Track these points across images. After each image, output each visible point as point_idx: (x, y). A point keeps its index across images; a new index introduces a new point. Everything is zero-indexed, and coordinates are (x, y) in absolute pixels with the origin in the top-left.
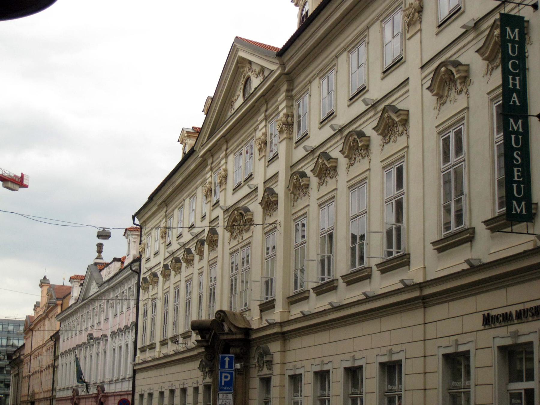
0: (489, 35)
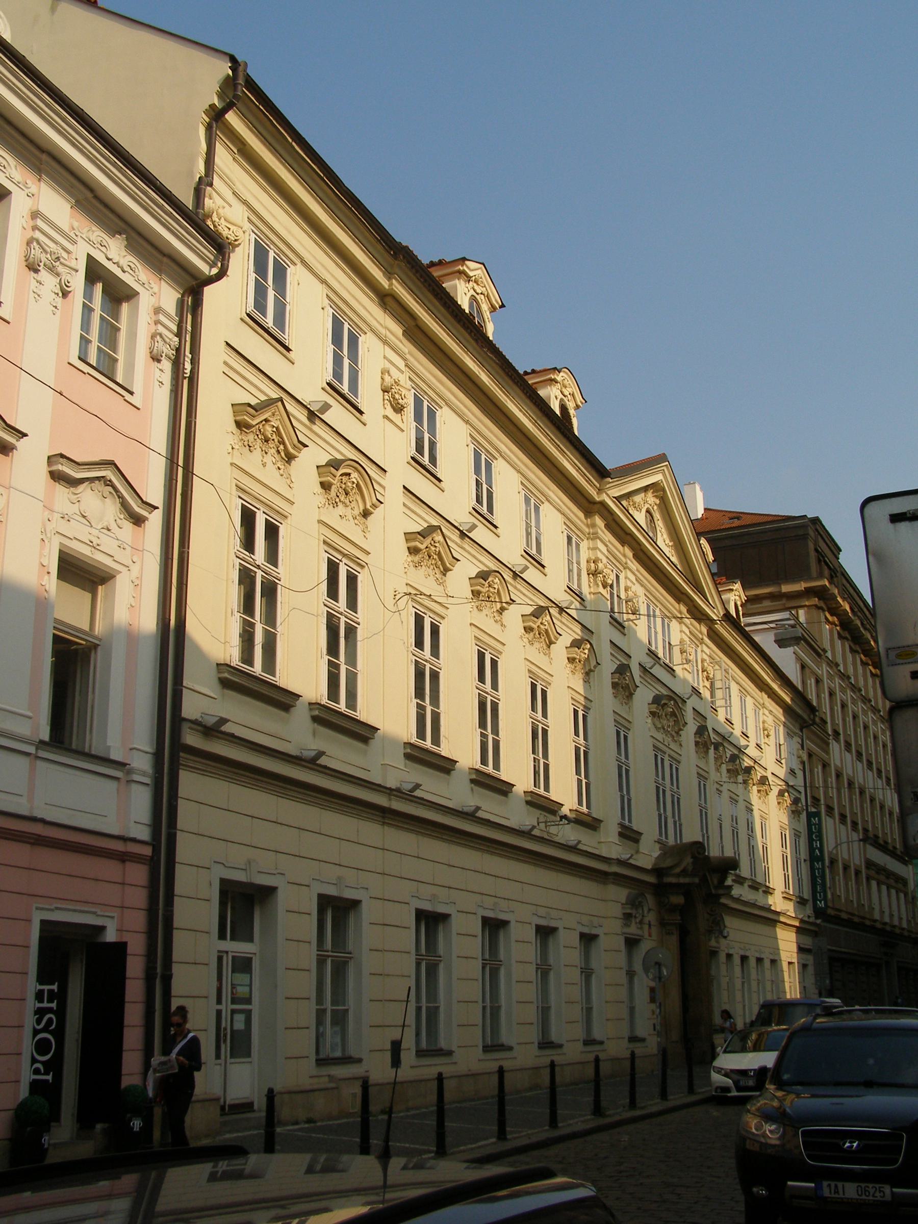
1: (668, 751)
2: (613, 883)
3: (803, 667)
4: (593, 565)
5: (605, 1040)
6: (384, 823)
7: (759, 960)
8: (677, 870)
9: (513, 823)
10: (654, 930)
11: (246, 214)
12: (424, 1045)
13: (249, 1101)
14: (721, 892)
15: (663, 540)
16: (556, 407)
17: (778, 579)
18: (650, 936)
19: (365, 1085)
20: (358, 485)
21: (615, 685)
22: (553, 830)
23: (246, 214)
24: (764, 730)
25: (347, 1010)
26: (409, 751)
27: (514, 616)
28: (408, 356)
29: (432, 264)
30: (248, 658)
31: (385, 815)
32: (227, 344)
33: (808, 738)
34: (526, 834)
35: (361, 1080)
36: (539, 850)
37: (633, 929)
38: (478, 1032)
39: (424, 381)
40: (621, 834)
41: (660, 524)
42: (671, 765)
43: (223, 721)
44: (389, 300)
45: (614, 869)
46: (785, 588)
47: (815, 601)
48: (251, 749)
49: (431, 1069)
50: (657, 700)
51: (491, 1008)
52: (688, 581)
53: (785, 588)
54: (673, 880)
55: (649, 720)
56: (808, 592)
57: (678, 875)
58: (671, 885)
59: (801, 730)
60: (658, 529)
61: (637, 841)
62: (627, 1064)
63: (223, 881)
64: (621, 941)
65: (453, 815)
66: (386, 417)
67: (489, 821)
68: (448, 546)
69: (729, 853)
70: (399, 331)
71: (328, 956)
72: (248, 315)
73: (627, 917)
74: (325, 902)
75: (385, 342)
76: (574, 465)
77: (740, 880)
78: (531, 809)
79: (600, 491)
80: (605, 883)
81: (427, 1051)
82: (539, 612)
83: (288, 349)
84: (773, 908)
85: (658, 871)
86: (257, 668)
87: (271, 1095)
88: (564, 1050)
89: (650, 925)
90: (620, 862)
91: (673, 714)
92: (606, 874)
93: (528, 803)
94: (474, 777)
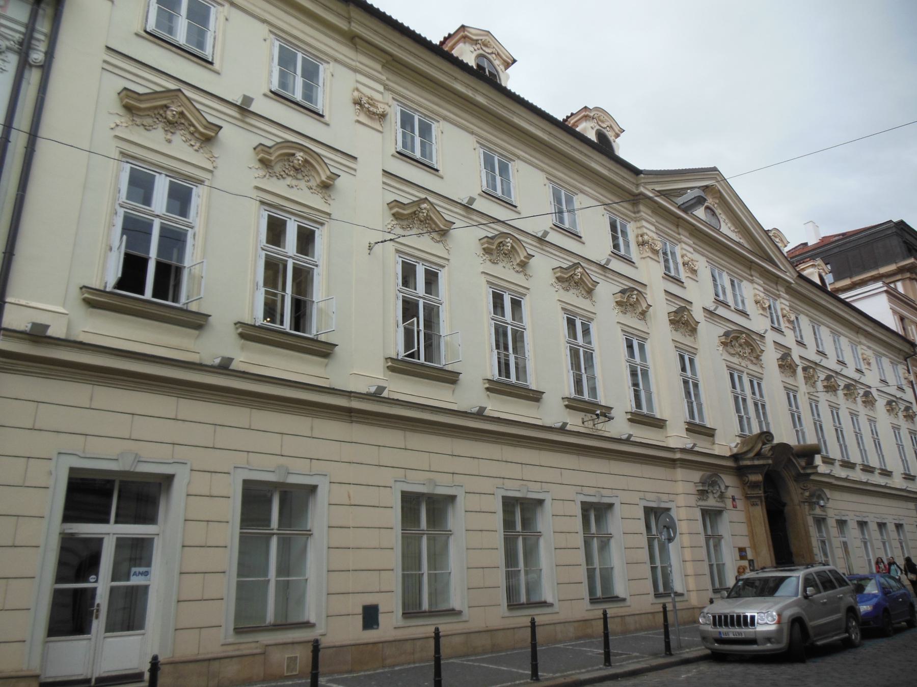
0: (414, 202)
1: (746, 371)
2: (681, 467)
3: (902, 319)
4: (640, 238)
5: (685, 593)
6: (352, 422)
7: (842, 523)
8: (751, 455)
9: (548, 422)
10: (740, 504)
11: (391, 96)
12: (717, 586)
13: (137, 671)
14: (809, 471)
15: (727, 229)
16: (592, 136)
17: (876, 266)
18: (735, 507)
19: (316, 647)
20: (306, 161)
21: (780, 366)
22: (599, 426)
23: (391, 96)
24: (864, 359)
25: (269, 581)
26: (390, 364)
27: (840, 393)
28: (387, 82)
29: (442, 43)
30: (638, 404)
31: (349, 415)
32: (108, 48)
33: (913, 365)
34: (562, 429)
35: (310, 644)
36: (381, 411)
37: (712, 502)
38: (708, 579)
39: (412, 101)
40: (687, 430)
41: (722, 217)
42: (751, 382)
43: (630, 436)
44: (357, 40)
45: (678, 456)
46: (883, 270)
47: (908, 275)
48: (18, 338)
49: (423, 628)
50: (889, 403)
51: (718, 565)
52: (760, 257)
53: (883, 270)
54: (748, 463)
55: (721, 348)
56: (901, 270)
57: (752, 459)
58: (747, 467)
59: (906, 360)
60: (721, 220)
61: (712, 436)
62: (660, 618)
63: (504, 498)
64: (698, 514)
65: (112, 354)
66: (358, 122)
67: (499, 418)
68: (198, 110)
69: (811, 439)
70: (379, 67)
71: (273, 534)
72: (398, 152)
73: (702, 494)
74: (509, 504)
75: (355, 70)
76: (543, 130)
77: (828, 461)
78: (572, 411)
79: (638, 185)
80: (674, 468)
81: (430, 612)
82: (828, 378)
83: (437, 170)
84: (50, 332)
85: (735, 457)
86: (513, 379)
87: (155, 665)
88: (628, 603)
89: (734, 499)
90: (683, 450)
91: (747, 344)
92: (674, 460)
93: (629, 420)
94: (487, 385)
